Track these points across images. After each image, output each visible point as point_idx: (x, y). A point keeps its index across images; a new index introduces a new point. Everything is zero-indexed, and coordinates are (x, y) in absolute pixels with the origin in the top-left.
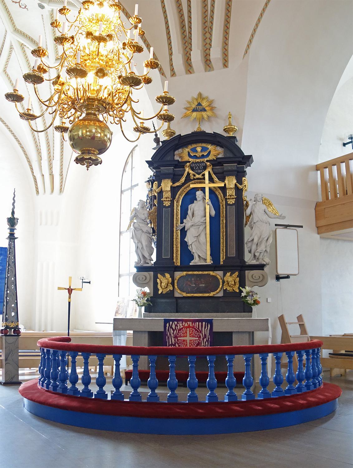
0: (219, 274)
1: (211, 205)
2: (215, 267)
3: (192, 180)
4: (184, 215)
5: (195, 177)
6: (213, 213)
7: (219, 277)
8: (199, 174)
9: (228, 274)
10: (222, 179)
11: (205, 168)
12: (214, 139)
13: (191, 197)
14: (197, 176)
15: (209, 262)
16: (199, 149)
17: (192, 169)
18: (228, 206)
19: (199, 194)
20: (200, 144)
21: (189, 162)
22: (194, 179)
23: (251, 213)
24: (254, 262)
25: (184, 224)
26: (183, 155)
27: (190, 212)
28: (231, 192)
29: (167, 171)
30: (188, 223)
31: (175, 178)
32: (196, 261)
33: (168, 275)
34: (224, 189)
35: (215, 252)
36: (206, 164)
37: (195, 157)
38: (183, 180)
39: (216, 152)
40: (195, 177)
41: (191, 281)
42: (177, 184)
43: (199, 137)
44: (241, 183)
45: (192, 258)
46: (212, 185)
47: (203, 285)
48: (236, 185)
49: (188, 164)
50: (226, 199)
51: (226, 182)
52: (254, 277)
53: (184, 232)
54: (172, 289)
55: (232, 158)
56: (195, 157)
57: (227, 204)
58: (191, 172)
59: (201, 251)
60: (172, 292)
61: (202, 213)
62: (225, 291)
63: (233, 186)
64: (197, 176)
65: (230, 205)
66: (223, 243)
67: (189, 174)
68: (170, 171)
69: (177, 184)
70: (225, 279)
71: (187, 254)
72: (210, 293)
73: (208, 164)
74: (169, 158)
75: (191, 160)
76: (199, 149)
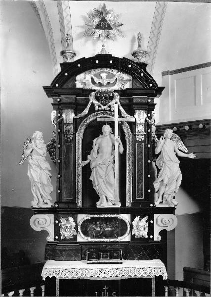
0: (126, 217)
1: (121, 142)
2: (123, 210)
3: (96, 111)
4: (87, 148)
5: (100, 109)
6: (122, 150)
7: (127, 221)
8: (104, 105)
9: (137, 218)
10: (132, 113)
11: (112, 98)
12: (121, 64)
13: (95, 130)
14: (103, 107)
15: (119, 205)
16: (104, 75)
17: (97, 98)
18: (136, 144)
19: (106, 128)
20: (105, 69)
21: (94, 91)
22: (99, 110)
23: (160, 153)
24: (164, 205)
25: (87, 162)
26: (83, 80)
27: (95, 148)
28: (140, 129)
29: (68, 101)
30: (93, 156)
31: (78, 108)
32: (102, 204)
33: (71, 219)
34: (132, 125)
35: (122, 198)
36: (113, 94)
37: (101, 85)
38: (86, 111)
39: (123, 81)
40: (100, 109)
41: (96, 225)
42: (79, 116)
43: (104, 61)
44: (150, 118)
45: (97, 198)
46: (121, 119)
47: (110, 229)
48: (146, 120)
49: (93, 93)
50: (135, 135)
51: (136, 116)
52: (163, 222)
53: (87, 170)
54: (75, 234)
55: (140, 89)
56: (101, 85)
57: (135, 141)
58: (96, 102)
59: (109, 196)
60: (75, 237)
61: (110, 149)
62: (133, 237)
63: (143, 121)
64: (103, 107)
65: (138, 142)
66: (130, 182)
67: (93, 104)
68: (71, 101)
69: (79, 116)
70: (134, 223)
71: (91, 195)
72: (117, 238)
73: (116, 94)
74: (70, 85)
75: (95, 88)
76: (104, 75)
